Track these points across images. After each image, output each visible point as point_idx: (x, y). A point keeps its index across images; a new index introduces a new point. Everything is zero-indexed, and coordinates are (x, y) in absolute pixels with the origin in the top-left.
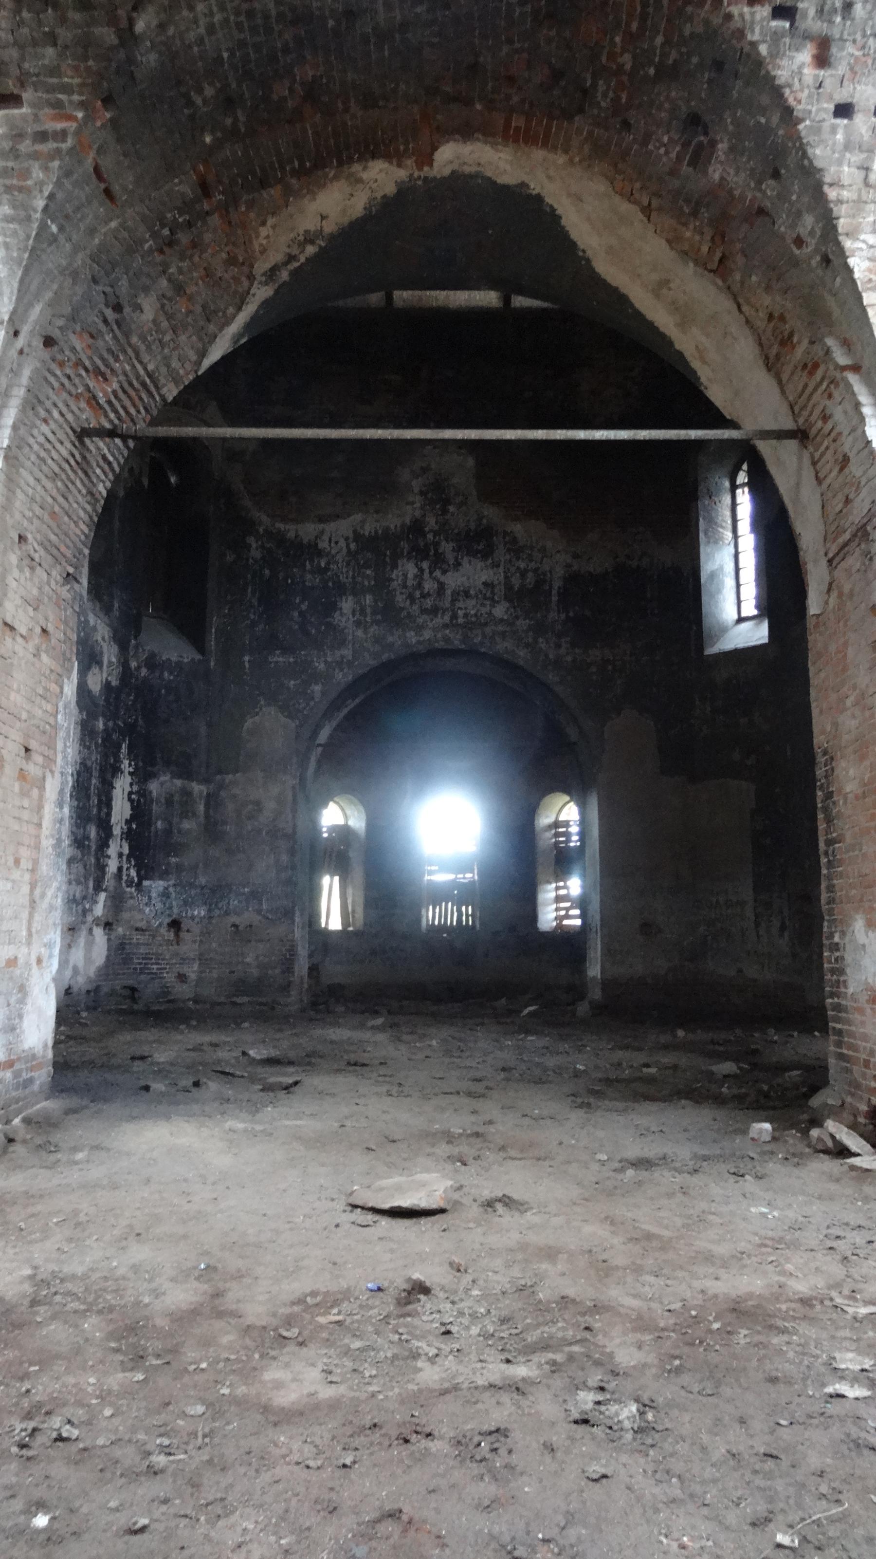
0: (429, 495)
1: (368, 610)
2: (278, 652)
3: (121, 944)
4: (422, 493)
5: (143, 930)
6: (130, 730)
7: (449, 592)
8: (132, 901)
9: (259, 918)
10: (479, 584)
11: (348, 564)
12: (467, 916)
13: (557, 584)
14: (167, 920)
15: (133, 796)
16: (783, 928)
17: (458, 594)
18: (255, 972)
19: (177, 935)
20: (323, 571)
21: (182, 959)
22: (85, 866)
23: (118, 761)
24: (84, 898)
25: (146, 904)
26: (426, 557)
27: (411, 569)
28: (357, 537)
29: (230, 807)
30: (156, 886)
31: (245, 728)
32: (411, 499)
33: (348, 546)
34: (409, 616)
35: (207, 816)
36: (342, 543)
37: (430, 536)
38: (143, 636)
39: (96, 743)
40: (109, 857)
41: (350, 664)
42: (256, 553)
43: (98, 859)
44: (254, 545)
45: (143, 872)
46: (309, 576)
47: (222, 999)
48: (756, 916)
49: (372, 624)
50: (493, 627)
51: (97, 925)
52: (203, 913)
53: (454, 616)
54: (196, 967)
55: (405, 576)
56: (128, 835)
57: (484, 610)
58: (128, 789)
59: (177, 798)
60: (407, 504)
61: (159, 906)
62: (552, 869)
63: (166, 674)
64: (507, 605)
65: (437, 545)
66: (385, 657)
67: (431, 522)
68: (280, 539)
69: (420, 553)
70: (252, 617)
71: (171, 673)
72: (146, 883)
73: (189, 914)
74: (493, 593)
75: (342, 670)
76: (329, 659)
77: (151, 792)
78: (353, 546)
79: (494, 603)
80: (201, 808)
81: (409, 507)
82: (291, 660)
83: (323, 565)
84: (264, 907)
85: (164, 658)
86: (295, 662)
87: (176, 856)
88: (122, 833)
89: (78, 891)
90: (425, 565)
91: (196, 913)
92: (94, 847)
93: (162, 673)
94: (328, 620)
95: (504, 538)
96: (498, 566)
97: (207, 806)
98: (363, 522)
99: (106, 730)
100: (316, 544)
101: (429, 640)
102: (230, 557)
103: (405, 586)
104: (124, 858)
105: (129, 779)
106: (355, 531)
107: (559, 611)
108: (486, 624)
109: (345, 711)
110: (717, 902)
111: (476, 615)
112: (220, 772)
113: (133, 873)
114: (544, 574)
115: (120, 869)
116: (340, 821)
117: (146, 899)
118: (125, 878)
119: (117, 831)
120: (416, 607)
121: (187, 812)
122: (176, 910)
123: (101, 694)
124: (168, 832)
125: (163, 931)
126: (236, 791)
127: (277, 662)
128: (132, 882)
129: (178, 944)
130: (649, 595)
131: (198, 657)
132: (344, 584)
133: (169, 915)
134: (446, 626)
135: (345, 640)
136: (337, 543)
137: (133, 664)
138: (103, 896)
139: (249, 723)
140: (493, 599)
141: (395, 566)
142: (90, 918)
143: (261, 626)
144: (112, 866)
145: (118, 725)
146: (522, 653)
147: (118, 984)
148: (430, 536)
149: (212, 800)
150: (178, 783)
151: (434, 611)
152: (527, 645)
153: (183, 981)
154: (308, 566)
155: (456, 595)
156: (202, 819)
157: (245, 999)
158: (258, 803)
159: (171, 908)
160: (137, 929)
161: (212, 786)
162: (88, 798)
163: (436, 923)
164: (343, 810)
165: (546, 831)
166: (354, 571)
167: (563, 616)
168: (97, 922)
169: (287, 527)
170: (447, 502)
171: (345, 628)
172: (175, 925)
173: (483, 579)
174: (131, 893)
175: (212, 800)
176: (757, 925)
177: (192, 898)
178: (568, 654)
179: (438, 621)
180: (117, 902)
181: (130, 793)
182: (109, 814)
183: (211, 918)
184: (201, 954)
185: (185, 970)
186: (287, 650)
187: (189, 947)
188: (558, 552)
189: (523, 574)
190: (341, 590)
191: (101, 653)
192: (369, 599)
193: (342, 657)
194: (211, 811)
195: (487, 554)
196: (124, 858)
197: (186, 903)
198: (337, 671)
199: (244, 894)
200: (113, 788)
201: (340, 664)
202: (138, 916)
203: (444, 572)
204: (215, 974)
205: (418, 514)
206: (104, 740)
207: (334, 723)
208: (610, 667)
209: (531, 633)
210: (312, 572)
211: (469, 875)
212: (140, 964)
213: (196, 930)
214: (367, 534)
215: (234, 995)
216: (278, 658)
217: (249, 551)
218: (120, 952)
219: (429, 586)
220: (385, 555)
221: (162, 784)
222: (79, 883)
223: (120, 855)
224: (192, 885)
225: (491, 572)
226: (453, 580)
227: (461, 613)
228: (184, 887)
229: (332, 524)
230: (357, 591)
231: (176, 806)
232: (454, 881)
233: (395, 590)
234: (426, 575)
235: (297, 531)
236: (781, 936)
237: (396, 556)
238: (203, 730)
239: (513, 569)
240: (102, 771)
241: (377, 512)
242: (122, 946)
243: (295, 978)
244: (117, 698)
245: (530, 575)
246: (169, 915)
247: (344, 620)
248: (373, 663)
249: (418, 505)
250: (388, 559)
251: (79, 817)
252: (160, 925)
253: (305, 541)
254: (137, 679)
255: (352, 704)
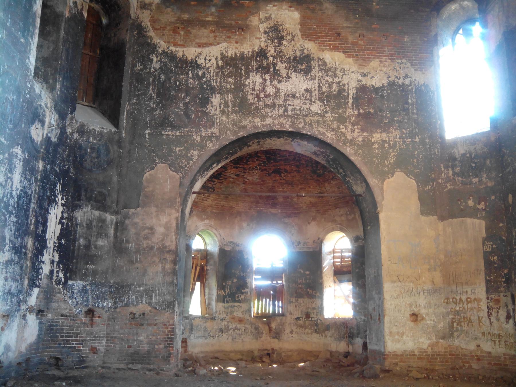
0: (271, 34)
1: (230, 104)
2: (168, 129)
3: (50, 326)
4: (265, 32)
5: (66, 316)
6: (65, 174)
7: (282, 94)
8: (59, 295)
9: (150, 308)
10: (302, 91)
11: (217, 75)
12: (279, 307)
13: (352, 92)
14: (85, 309)
15: (64, 221)
16: (508, 317)
17: (289, 96)
18: (146, 347)
19: (92, 320)
20: (199, 78)
21: (95, 337)
22: (21, 268)
23: (53, 194)
24: (20, 291)
25: (70, 297)
26: (268, 72)
27: (258, 79)
28: (223, 57)
29: (132, 231)
30: (77, 284)
31: (144, 177)
32: (258, 36)
33: (217, 63)
34: (256, 108)
35: (116, 237)
36: (214, 61)
37: (271, 59)
38: (76, 113)
39: (36, 178)
40: (43, 262)
41: (217, 138)
42: (156, 65)
43: (33, 264)
44: (155, 60)
45: (68, 275)
46: (191, 81)
47: (122, 366)
48: (489, 308)
49: (232, 113)
50: (311, 118)
51: (31, 312)
52: (110, 304)
53: (286, 110)
54: (104, 342)
55: (254, 83)
56: (59, 248)
57: (305, 107)
58: (60, 215)
59: (94, 224)
60: (257, 38)
61: (79, 299)
62: (332, 278)
63: (91, 139)
64: (320, 104)
65: (275, 65)
66: (241, 134)
67: (271, 51)
68: (172, 57)
69: (264, 69)
70: (152, 105)
71: (95, 138)
72: (70, 282)
73: (101, 305)
74: (311, 96)
75: (211, 141)
76: (203, 134)
77: (76, 219)
78: (220, 63)
79: (311, 102)
80: (112, 231)
81: (258, 41)
82: (178, 134)
83: (200, 74)
84: (154, 301)
85: (90, 128)
86: (181, 136)
87: (93, 263)
88: (55, 246)
89: (14, 287)
90: (267, 77)
91: (105, 304)
92: (29, 255)
93: (89, 137)
94: (204, 109)
95: (318, 62)
96: (314, 79)
97: (116, 230)
98: (228, 48)
99: (45, 171)
100: (196, 61)
101: (270, 124)
102: (139, 67)
103: (254, 90)
104: (55, 264)
105: (61, 208)
106: (222, 54)
107: (353, 109)
108: (306, 116)
109: (211, 172)
110: (461, 299)
111: (300, 110)
112: (125, 207)
113: (61, 275)
114: (344, 85)
115: (51, 272)
116: (202, 247)
117: (69, 294)
118: (55, 278)
119: (50, 244)
120: (261, 103)
121: (102, 233)
122: (91, 302)
123: (42, 145)
124: (87, 247)
125: (82, 316)
126: (136, 220)
127: (167, 135)
128: (60, 281)
129: (92, 327)
130: (410, 101)
131: (114, 129)
132: (214, 86)
133: (86, 306)
134: (280, 116)
135: (214, 123)
136: (210, 60)
137: (69, 130)
138: (36, 290)
139: (147, 175)
140: (311, 100)
141: (247, 77)
142: (23, 307)
143: (158, 111)
144: (46, 269)
145: (56, 171)
146: (330, 134)
147: (46, 356)
148: (271, 59)
149: (120, 227)
150: (97, 213)
151: (273, 106)
152: (333, 130)
153: (94, 353)
154: (190, 75)
155: (287, 97)
156: (112, 239)
157: (139, 366)
158: (151, 229)
159: (87, 301)
160: (62, 316)
161: (119, 217)
162: (27, 216)
163: (260, 312)
164: (204, 240)
165: (328, 255)
166: (221, 80)
167: (356, 112)
168: (30, 310)
169: (177, 49)
170: (282, 38)
171: (215, 114)
172: (90, 312)
173: (305, 87)
174: (59, 289)
175: (120, 227)
176: (489, 314)
177: (103, 294)
178: (359, 136)
179: (276, 113)
180: (48, 295)
181: (62, 218)
182: (44, 231)
183: (116, 308)
184: (108, 334)
185: (96, 344)
186: (174, 127)
187: (100, 327)
188: (353, 72)
189: (330, 85)
190: (212, 90)
191: (44, 116)
192: (230, 96)
193: (212, 133)
194: (118, 234)
195: (308, 71)
196: (55, 264)
197: (98, 297)
198: (208, 142)
199: (139, 291)
200: (48, 213)
201: (210, 138)
202: (63, 306)
203: (280, 82)
204: (118, 347)
205: (263, 45)
206: (42, 179)
207: (205, 179)
208: (386, 145)
209: (335, 122)
210: (193, 78)
211: (280, 282)
212: (64, 340)
213: (105, 316)
214: (230, 55)
215: (130, 363)
216: (168, 132)
217: (152, 63)
218: (49, 333)
219: (270, 90)
220: (241, 69)
221: (84, 213)
222: (14, 280)
223: (52, 262)
224: (103, 285)
225: (310, 83)
226: (285, 87)
227: (290, 108)
228: (97, 286)
229: (207, 48)
230: (222, 92)
231: (94, 229)
232: (271, 285)
233: (248, 92)
234: (268, 82)
235: (183, 52)
236: (507, 322)
237: (248, 72)
238: (115, 179)
239: (324, 82)
240: (40, 200)
241: (237, 43)
242: (50, 328)
243: (173, 351)
244: (55, 151)
245: (335, 85)
246: (86, 306)
247: (213, 110)
248: (234, 138)
249: (263, 39)
250: (243, 72)
251: (18, 230)
252: (79, 312)
253: (189, 59)
254: (71, 141)
255: (216, 168)
